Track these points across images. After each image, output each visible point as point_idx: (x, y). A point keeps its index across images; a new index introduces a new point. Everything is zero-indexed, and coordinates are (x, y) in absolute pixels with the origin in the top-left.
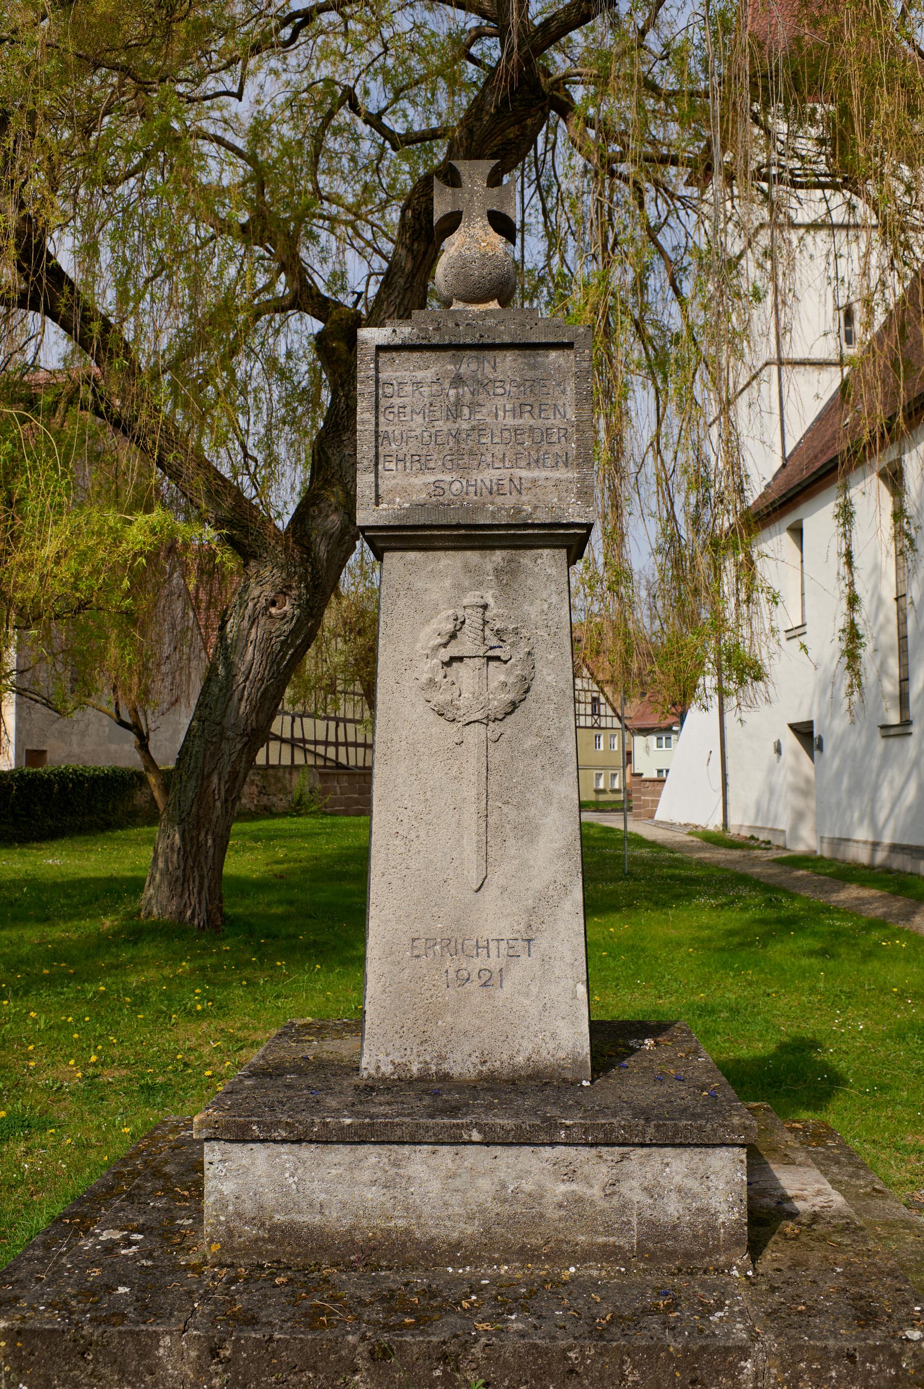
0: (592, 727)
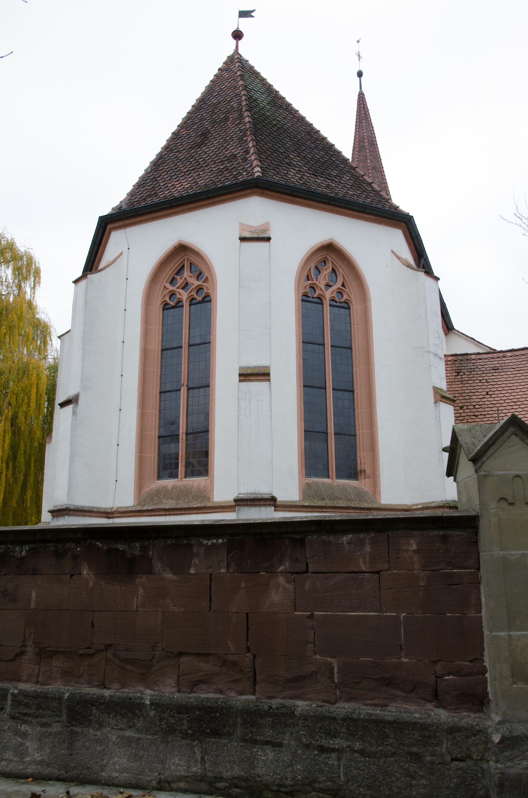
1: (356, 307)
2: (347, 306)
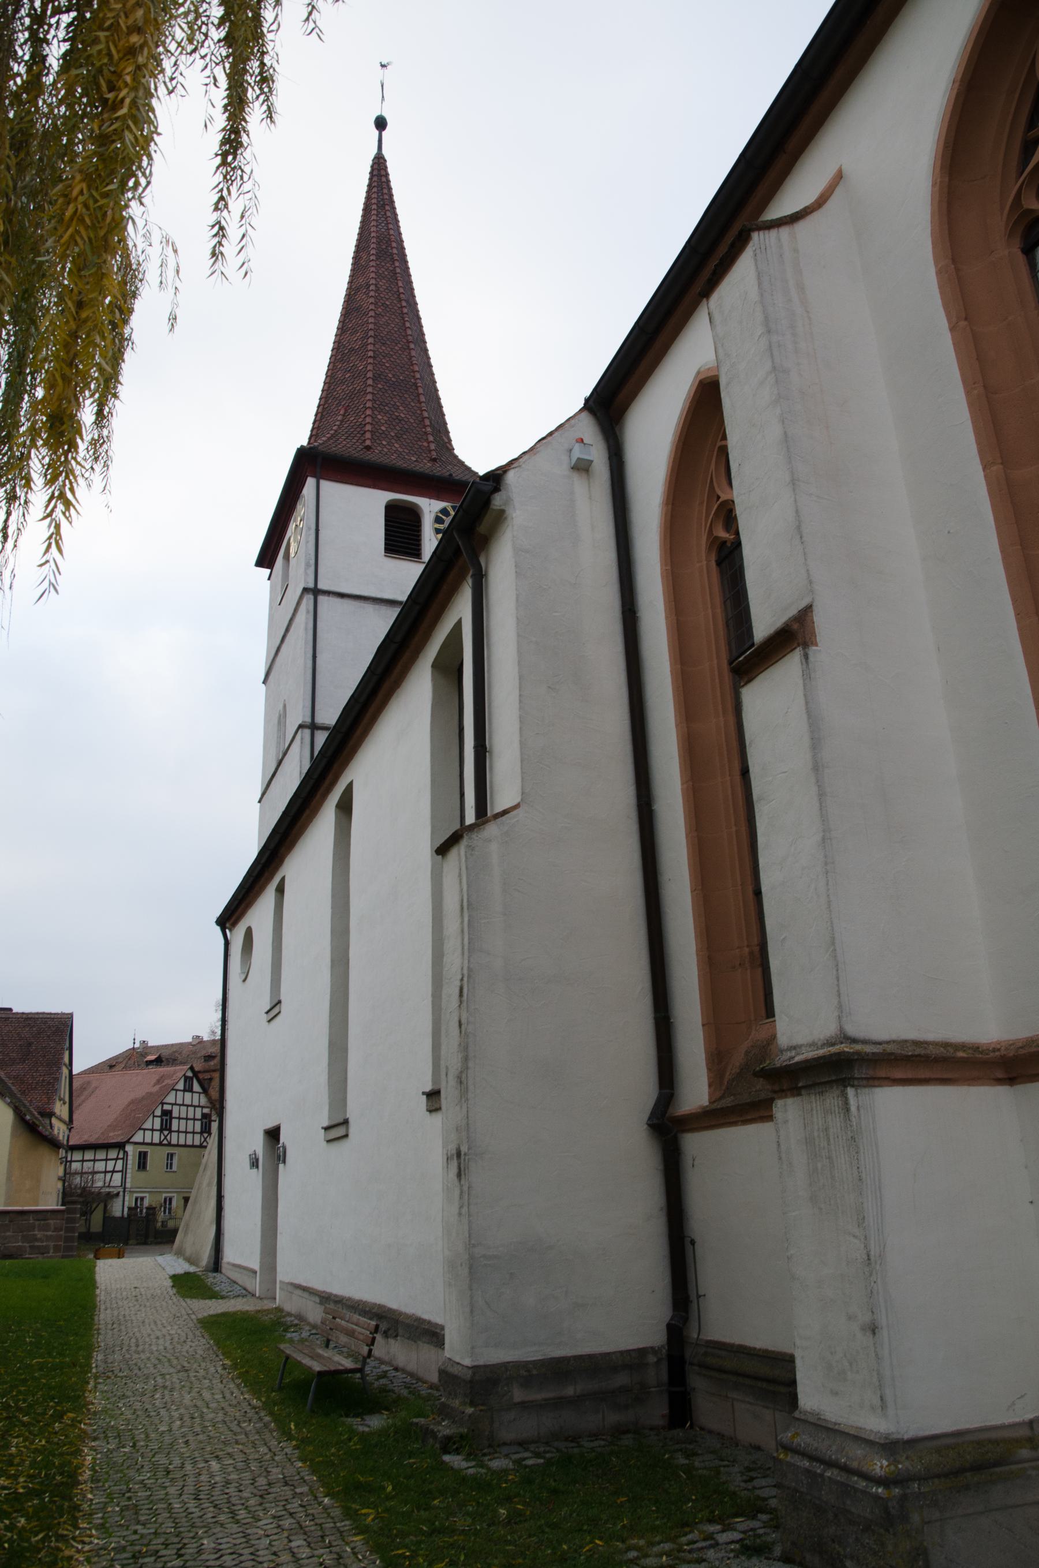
0: (160, 1144)
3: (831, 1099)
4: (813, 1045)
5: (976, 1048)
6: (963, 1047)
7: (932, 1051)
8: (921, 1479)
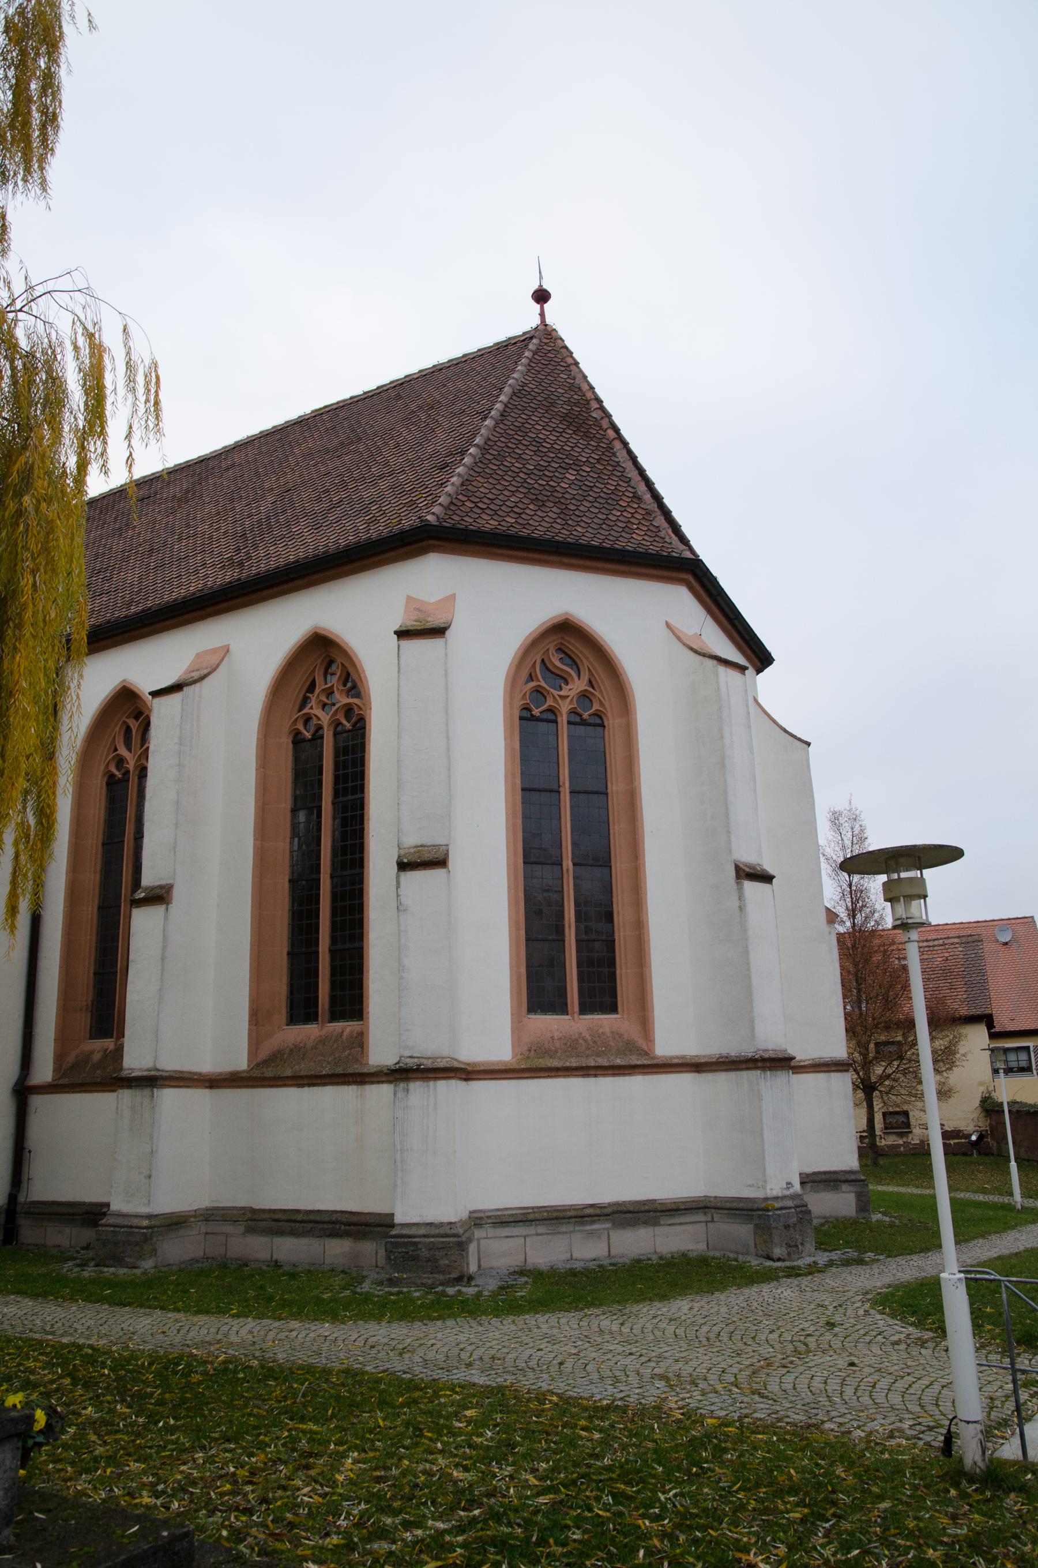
1: (613, 722)
2: (599, 722)
3: (147, 1092)
4: (140, 1069)
5: (200, 1074)
6: (196, 1074)
7: (186, 1075)
8: (158, 1227)
